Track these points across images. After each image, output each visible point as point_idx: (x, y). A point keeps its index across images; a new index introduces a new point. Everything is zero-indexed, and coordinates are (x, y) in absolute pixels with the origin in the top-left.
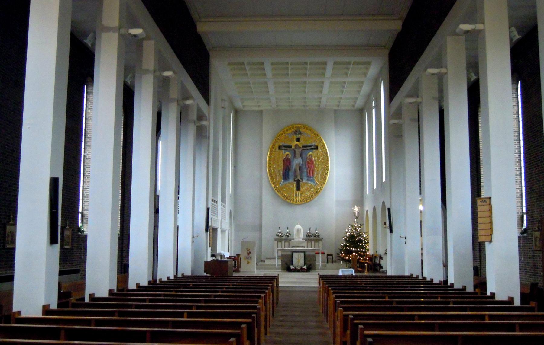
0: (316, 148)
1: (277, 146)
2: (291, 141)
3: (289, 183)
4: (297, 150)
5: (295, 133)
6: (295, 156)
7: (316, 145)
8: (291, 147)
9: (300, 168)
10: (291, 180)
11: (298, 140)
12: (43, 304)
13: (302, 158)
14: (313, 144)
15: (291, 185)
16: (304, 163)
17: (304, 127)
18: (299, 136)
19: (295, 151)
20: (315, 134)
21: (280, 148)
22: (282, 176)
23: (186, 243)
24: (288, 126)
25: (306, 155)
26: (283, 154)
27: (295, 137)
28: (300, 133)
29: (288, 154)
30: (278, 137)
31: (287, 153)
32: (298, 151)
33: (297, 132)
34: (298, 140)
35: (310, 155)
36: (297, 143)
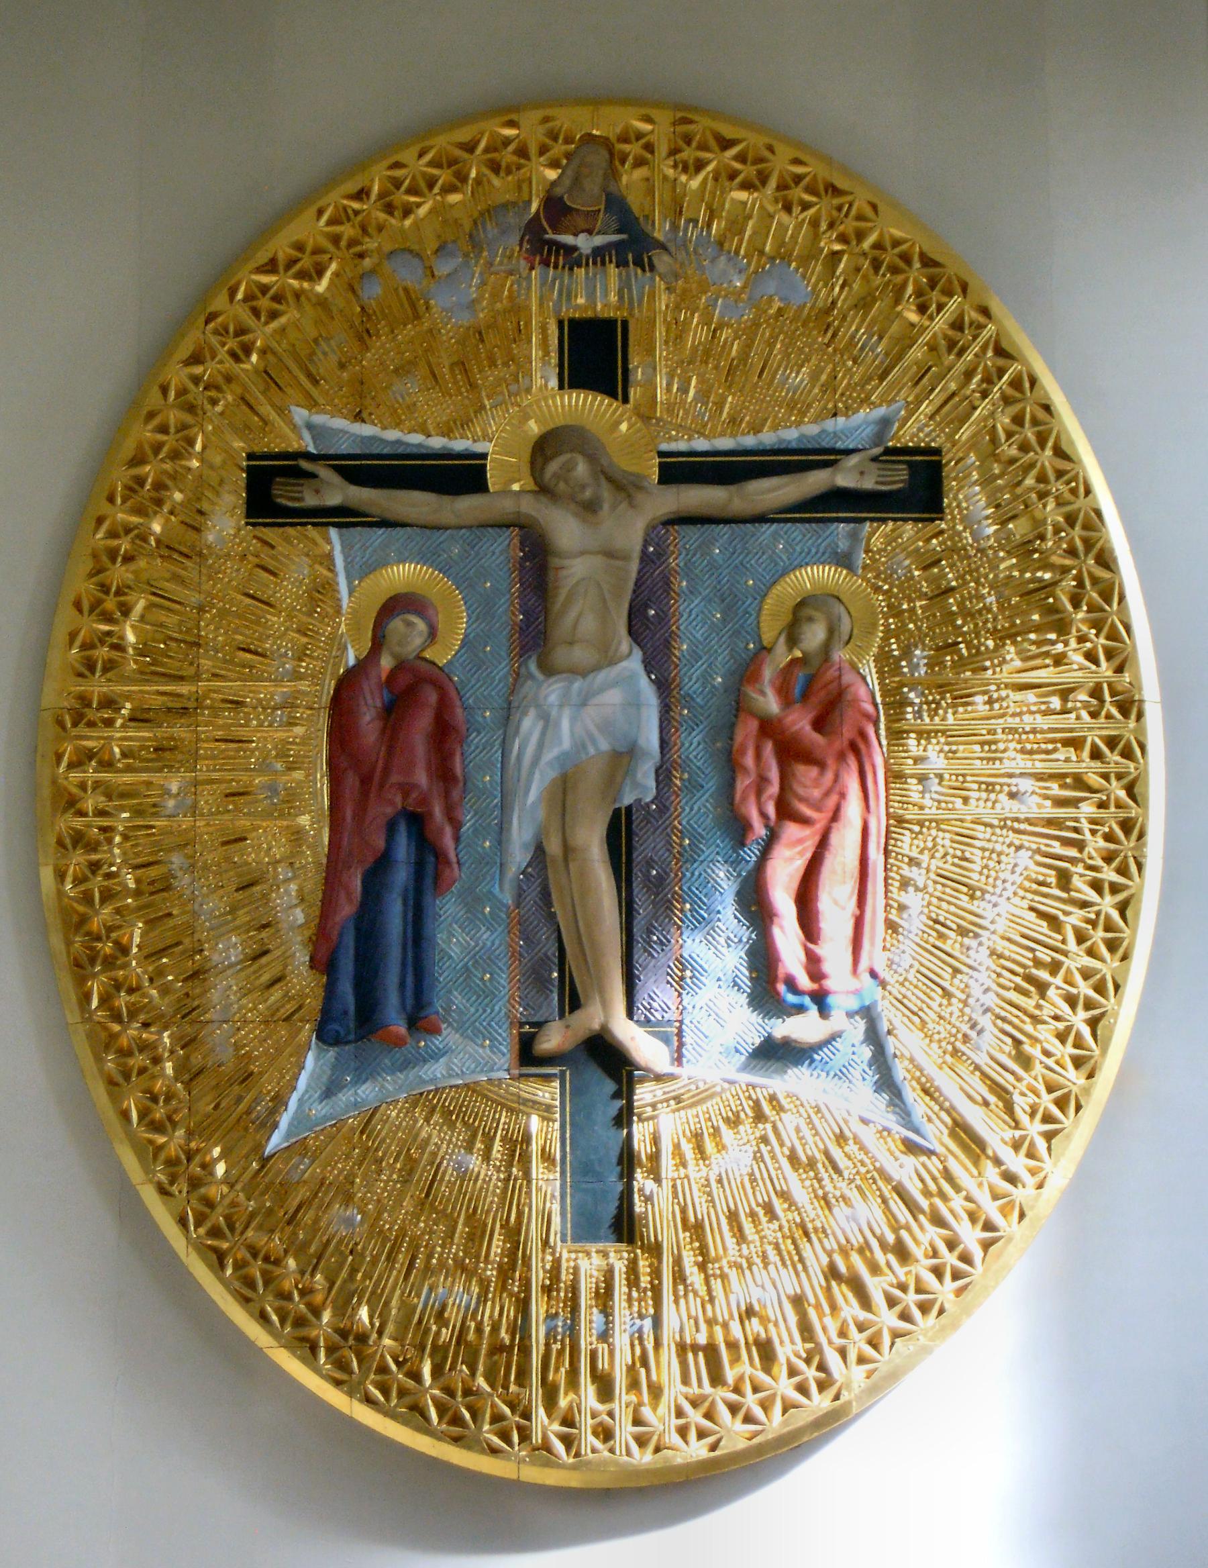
0: (920, 487)
1: (217, 453)
2: (477, 362)
3: (425, 1101)
4: (565, 530)
5: (544, 238)
6: (534, 634)
7: (914, 430)
8: (464, 476)
9: (621, 834)
10: (467, 1054)
11: (595, 356)
12: (872, 1091)
13: (658, 663)
14: (855, 425)
15: (477, 1136)
16: (693, 745)
17: (698, 133)
18: (599, 294)
19: (536, 559)
20: (891, 260)
21: (271, 488)
22: (304, 982)
23: (853, 808)
24: (420, 134)
25: (735, 606)
26: (322, 591)
27: (550, 301)
28: (634, 247)
29: (398, 604)
30: (214, 325)
31: (403, 574)
32: (592, 553)
33: (587, 217)
34: (595, 356)
35: (802, 611)
36: (585, 405)
